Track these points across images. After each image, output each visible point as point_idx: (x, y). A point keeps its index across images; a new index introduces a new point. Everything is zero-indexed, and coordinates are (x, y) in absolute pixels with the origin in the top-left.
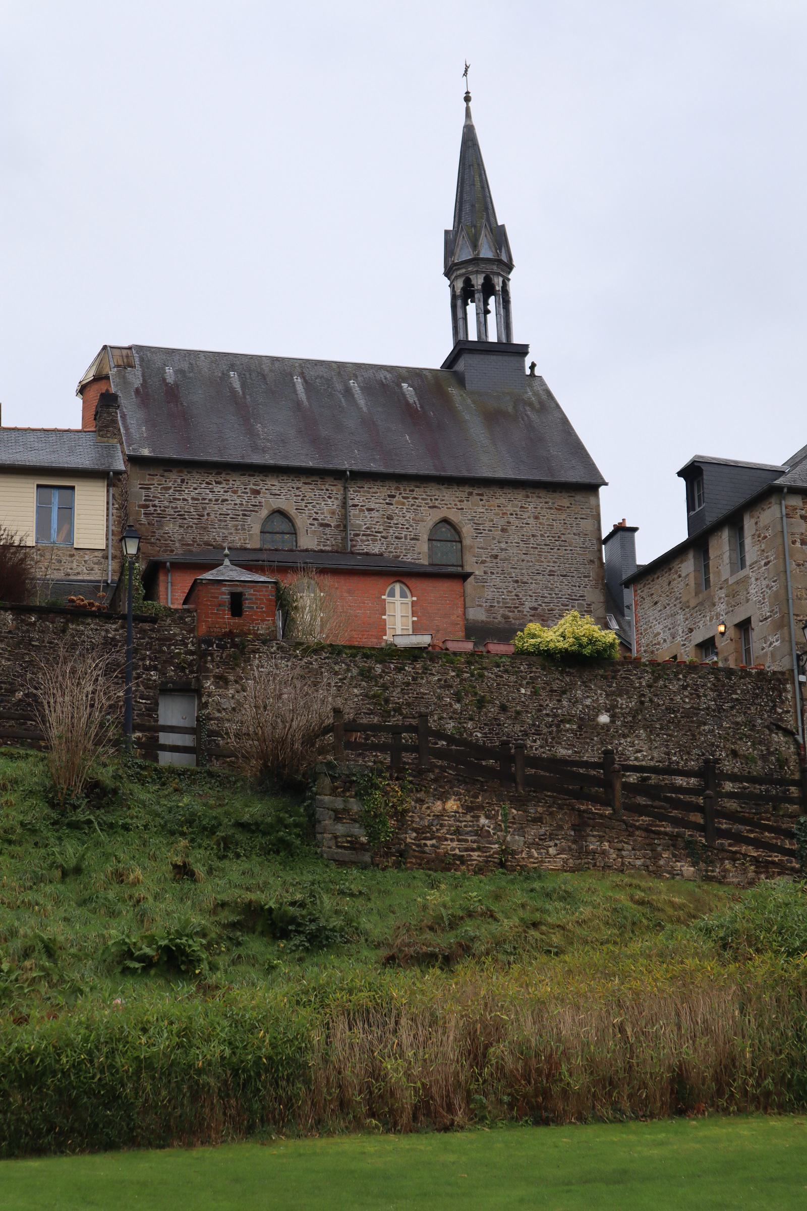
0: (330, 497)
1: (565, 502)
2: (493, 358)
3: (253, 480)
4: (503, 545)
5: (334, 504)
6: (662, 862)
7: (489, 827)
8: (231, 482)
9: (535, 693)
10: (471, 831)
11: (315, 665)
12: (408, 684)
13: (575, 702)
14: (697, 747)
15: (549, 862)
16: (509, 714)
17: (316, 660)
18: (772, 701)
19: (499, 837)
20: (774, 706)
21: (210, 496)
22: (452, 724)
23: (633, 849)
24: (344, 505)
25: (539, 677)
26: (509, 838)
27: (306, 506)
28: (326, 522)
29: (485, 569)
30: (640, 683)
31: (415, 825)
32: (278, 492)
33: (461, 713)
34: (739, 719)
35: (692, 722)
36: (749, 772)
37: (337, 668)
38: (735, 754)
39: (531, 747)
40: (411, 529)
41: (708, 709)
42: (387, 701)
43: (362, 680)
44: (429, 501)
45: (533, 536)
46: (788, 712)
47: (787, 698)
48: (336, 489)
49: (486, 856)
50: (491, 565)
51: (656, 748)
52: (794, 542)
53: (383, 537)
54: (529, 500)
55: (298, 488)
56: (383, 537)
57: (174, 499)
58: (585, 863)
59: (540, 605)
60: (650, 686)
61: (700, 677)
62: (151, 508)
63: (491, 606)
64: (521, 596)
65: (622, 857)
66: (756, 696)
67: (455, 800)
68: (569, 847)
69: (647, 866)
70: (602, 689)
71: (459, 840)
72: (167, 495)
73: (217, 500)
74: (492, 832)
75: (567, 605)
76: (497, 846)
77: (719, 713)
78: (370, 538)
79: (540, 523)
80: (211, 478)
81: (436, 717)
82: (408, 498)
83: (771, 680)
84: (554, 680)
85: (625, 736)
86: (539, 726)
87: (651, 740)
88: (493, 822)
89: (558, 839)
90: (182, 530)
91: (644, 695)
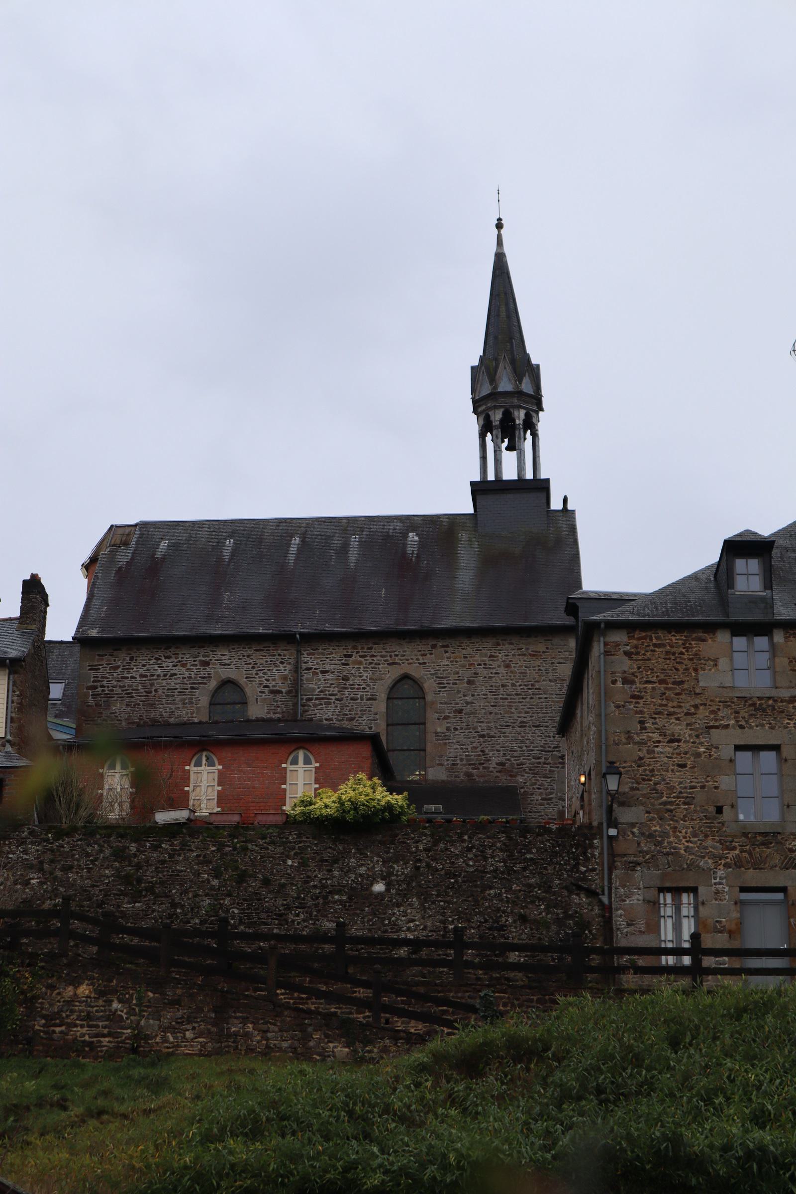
0: (282, 663)
1: (541, 648)
2: (510, 496)
3: (202, 651)
4: (469, 699)
5: (285, 670)
6: (311, 1044)
7: (122, 1011)
8: (181, 656)
9: (303, 864)
10: (102, 1016)
11: (67, 849)
12: (163, 862)
13: (348, 871)
14: (480, 913)
15: (185, 1046)
16: (272, 888)
17: (68, 842)
18: (574, 859)
19: (132, 1022)
20: (576, 866)
21: (159, 672)
22: (208, 901)
23: (280, 1031)
24: (297, 669)
25: (309, 847)
26: (142, 1023)
27: (257, 674)
28: (277, 688)
29: (448, 725)
30: (417, 847)
31: (44, 1012)
32: (228, 662)
33: (219, 889)
34: (532, 881)
35: (476, 886)
36: (540, 939)
37: (89, 850)
38: (523, 919)
39: (293, 921)
40: (368, 689)
41: (495, 871)
42: (139, 881)
43: (115, 861)
44: (388, 658)
45: (503, 686)
46: (594, 870)
47: (593, 855)
48: (289, 654)
49: (117, 1042)
50: (454, 720)
51: (430, 916)
52: (614, 682)
53: (337, 699)
54: (499, 648)
55: (248, 656)
56: (337, 699)
57: (123, 678)
58: (226, 1047)
59: (509, 760)
60: (427, 850)
61: (488, 837)
62: (100, 689)
63: (453, 764)
64: (487, 751)
65: (267, 1039)
66: (555, 854)
67: (87, 985)
68: (209, 1030)
69: (295, 1048)
70: (379, 856)
71: (89, 1026)
72: (115, 675)
73: (165, 675)
74: (125, 1016)
75: (539, 758)
76: (129, 1031)
77: (509, 875)
78: (323, 701)
79: (511, 672)
80: (160, 653)
81: (191, 895)
82: (366, 656)
83: (574, 836)
84: (326, 849)
85: (398, 905)
86: (304, 899)
87: (425, 909)
88: (127, 1006)
89: (197, 1022)
90: (129, 709)
91: (420, 860)
